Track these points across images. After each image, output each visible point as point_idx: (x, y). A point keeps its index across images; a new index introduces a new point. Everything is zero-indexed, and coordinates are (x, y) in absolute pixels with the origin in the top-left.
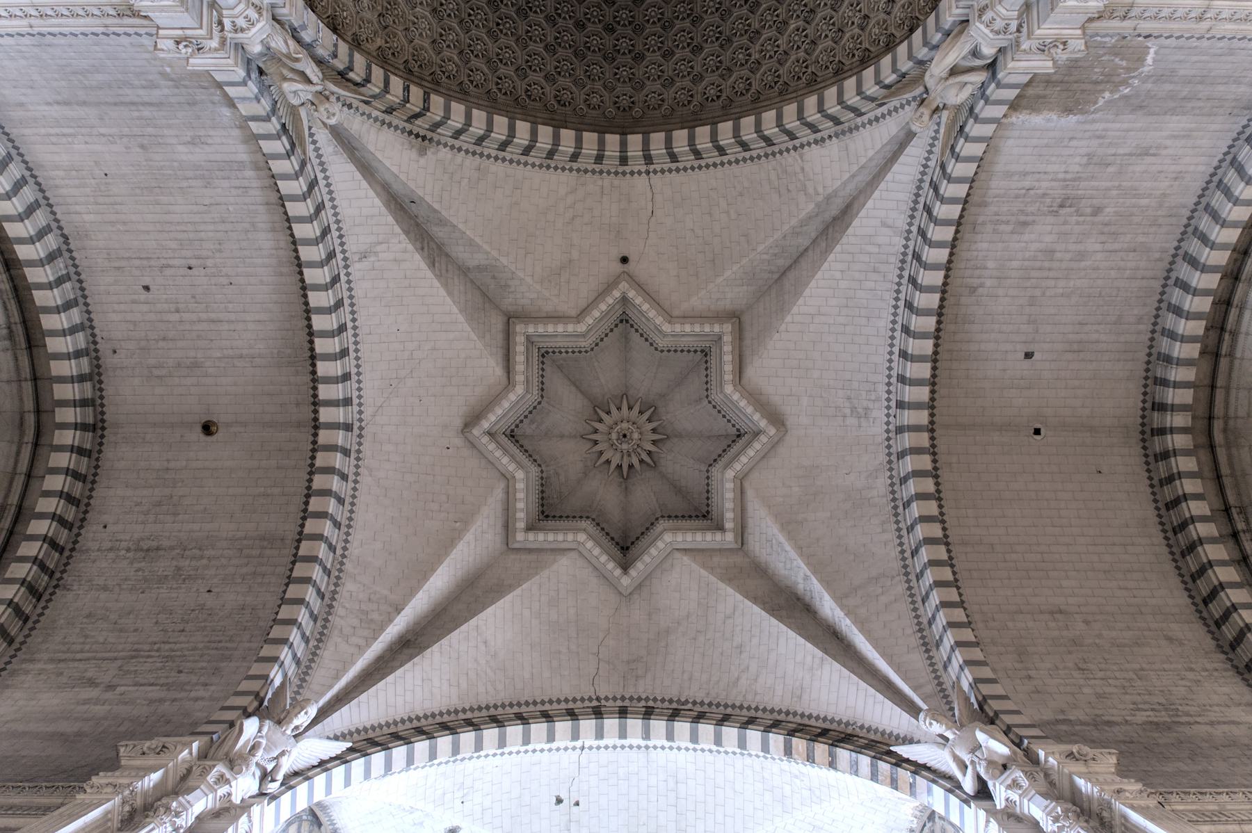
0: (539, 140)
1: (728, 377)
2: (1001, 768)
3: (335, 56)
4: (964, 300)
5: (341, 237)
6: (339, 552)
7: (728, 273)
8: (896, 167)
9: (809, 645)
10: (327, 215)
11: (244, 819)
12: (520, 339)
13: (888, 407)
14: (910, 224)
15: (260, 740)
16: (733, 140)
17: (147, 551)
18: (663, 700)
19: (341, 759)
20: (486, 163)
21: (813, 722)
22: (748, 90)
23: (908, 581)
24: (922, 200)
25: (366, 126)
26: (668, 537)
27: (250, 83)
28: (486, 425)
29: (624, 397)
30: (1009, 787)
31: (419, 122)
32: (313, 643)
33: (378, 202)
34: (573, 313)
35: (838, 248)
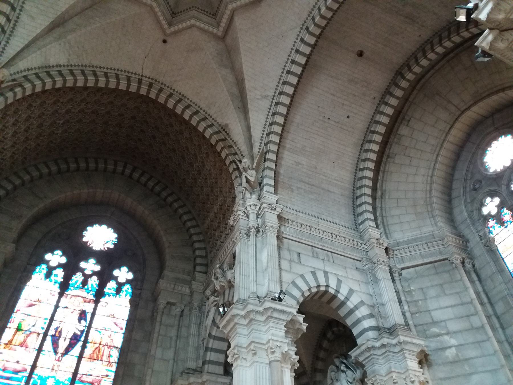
0: (181, 109)
10: (270, 120)
12: (221, 29)
16: (99, 79)
17: (411, 19)
20: (206, 109)
22: (89, 93)
24: (11, 25)
31: (223, 137)
34: (194, 29)
35: (59, 13)
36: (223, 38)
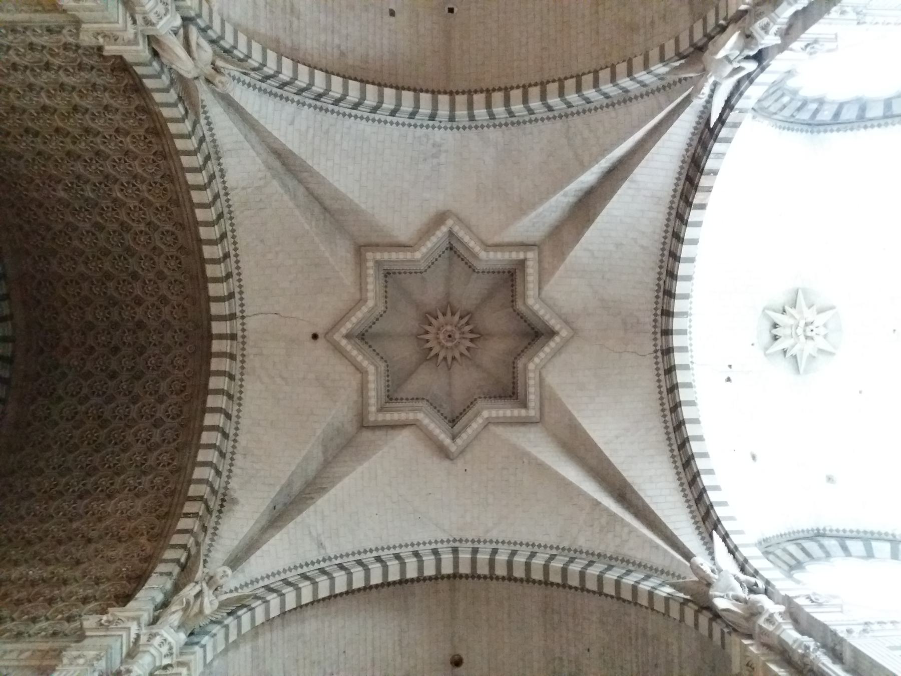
1: (409, 256)
2: (749, 39)
3: (169, 574)
4: (350, 62)
5: (307, 565)
6: (554, 552)
7: (327, 254)
8: (249, 109)
9: (619, 192)
11: (797, 601)
12: (381, 417)
13: (433, 127)
14: (293, 101)
15: (730, 596)
18: (656, 303)
19: (725, 537)
21: (680, 188)
23: (572, 114)
24: (275, 90)
25: (218, 547)
26: (530, 301)
27: (203, 642)
28: (447, 441)
29: (420, 337)
30: (767, 32)
31: (211, 504)
32: (631, 567)
33: (278, 536)
34: (359, 375)
35: (310, 162)
36: (363, 424)
